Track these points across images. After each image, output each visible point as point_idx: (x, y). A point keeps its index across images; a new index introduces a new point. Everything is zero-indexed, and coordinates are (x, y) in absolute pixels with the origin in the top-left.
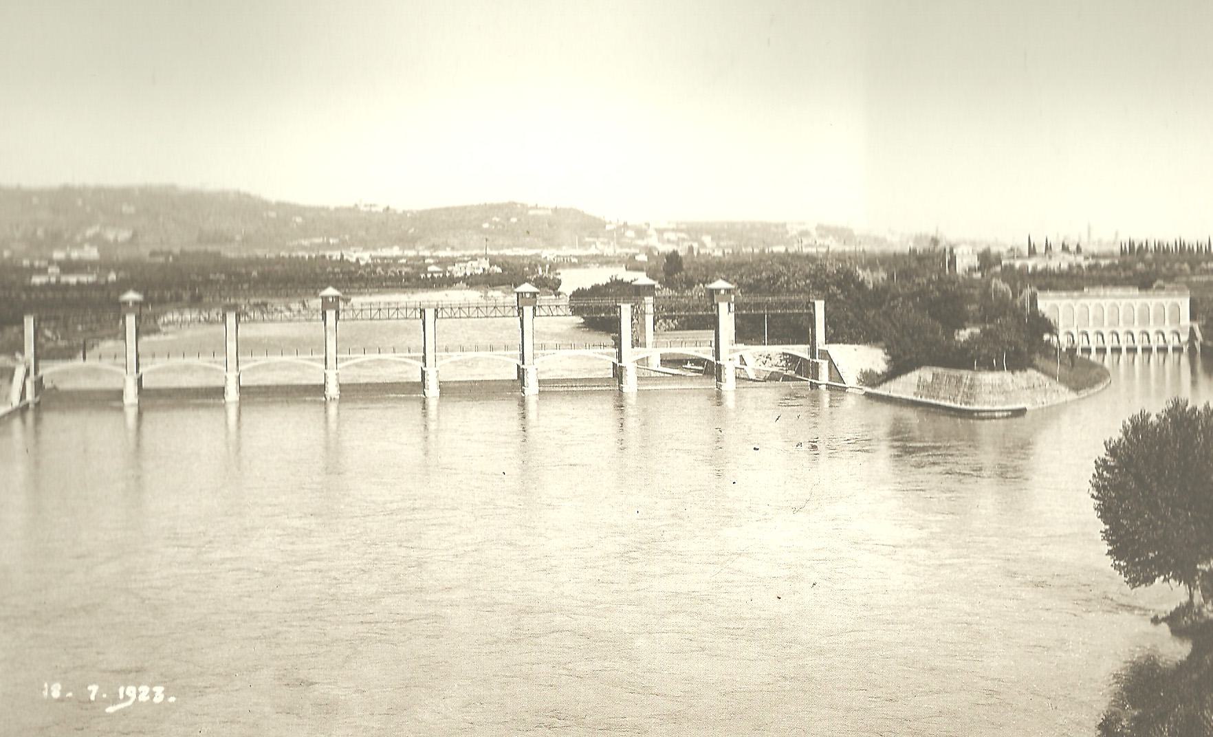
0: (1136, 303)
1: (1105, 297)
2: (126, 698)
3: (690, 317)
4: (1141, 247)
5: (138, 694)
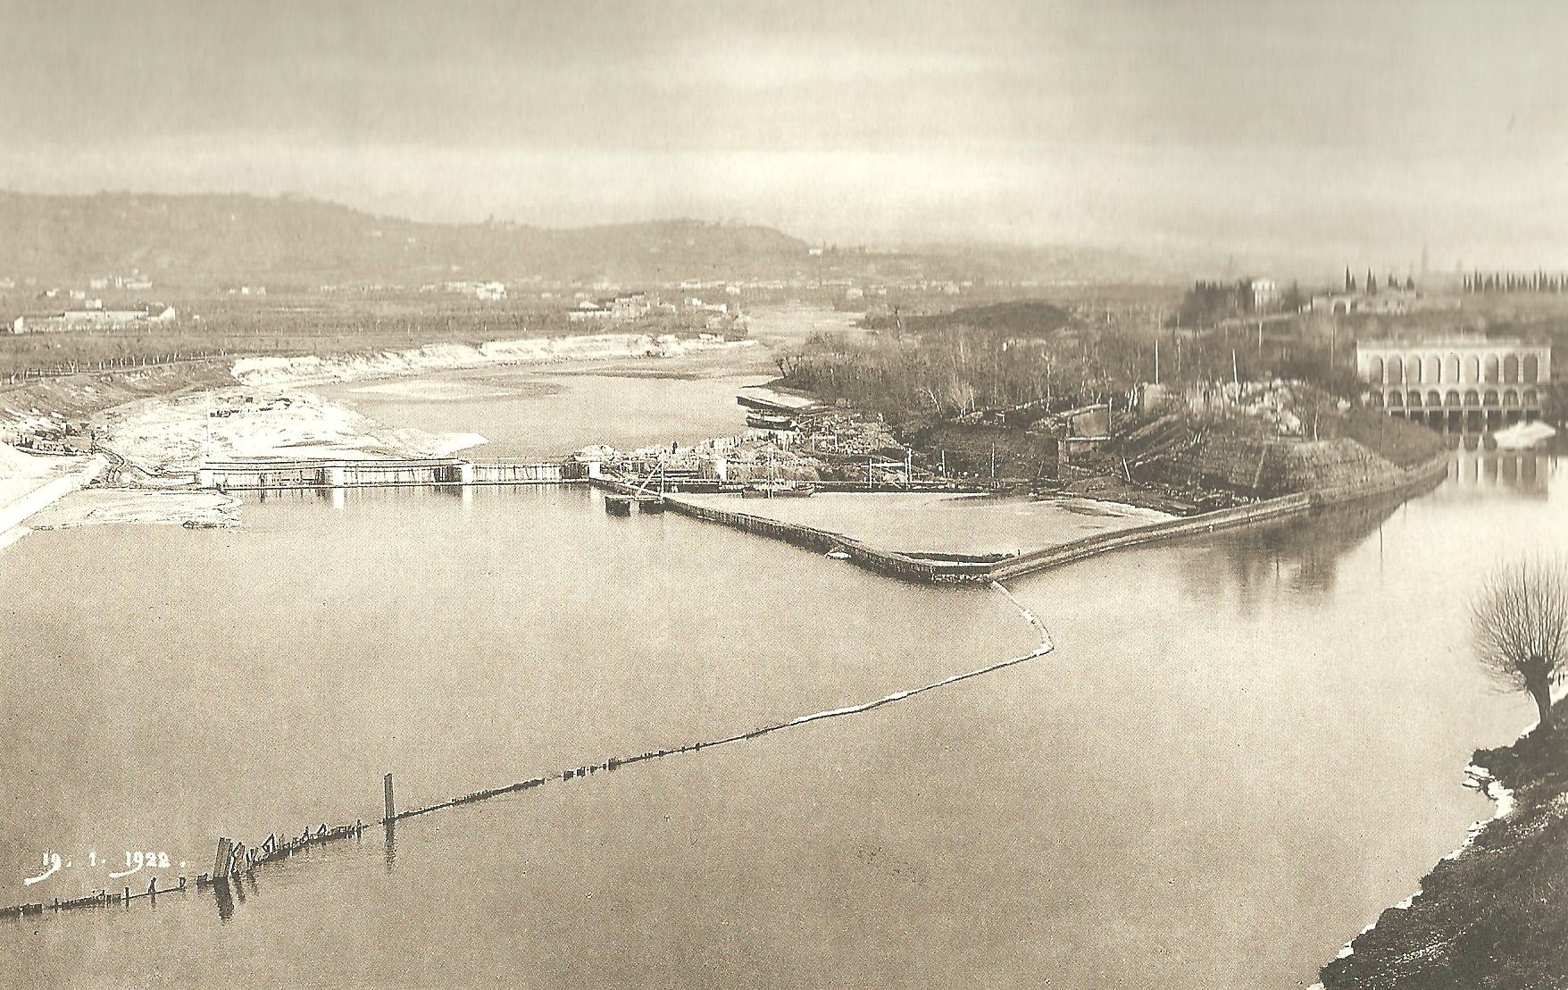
0: (1482, 355)
1: (1443, 346)
2: (134, 865)
3: (1262, 379)
4: (1490, 280)
5: (145, 861)
